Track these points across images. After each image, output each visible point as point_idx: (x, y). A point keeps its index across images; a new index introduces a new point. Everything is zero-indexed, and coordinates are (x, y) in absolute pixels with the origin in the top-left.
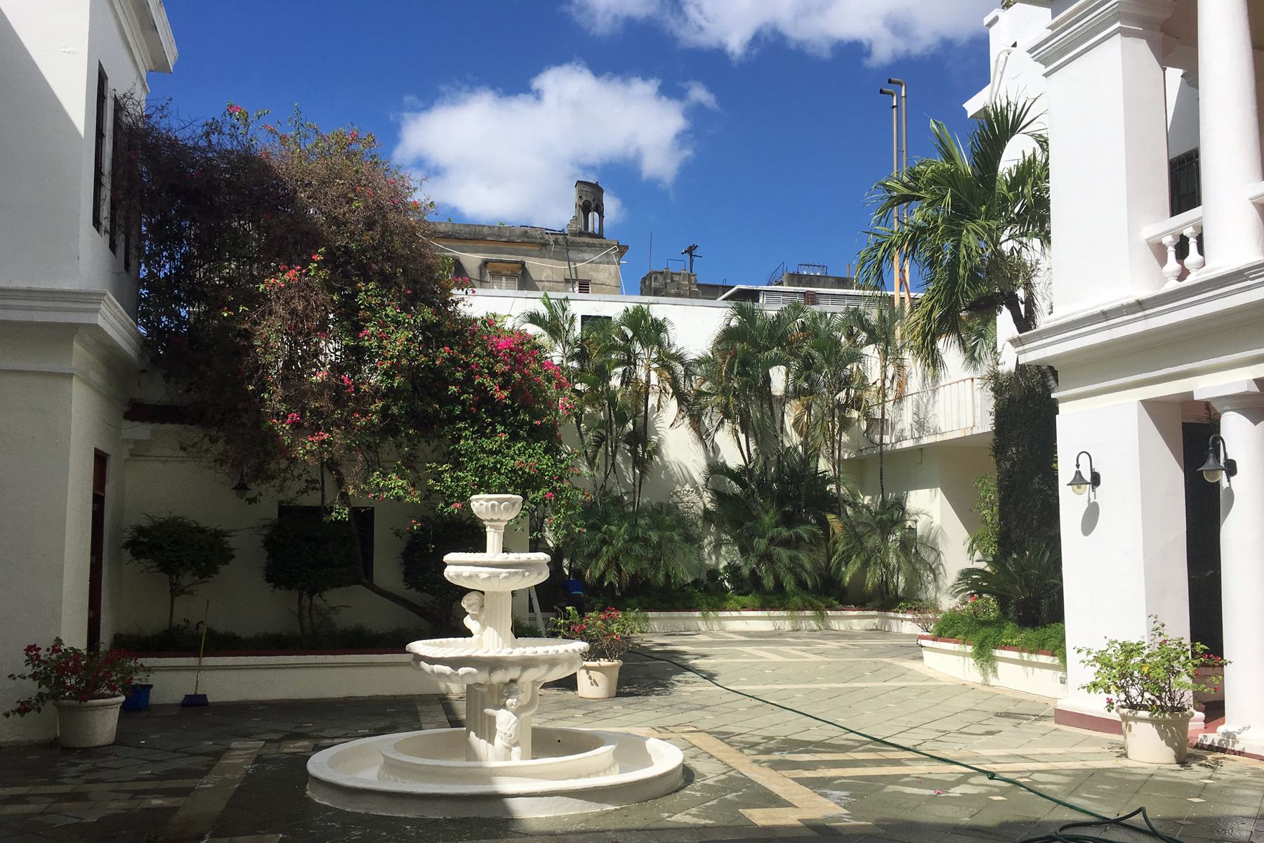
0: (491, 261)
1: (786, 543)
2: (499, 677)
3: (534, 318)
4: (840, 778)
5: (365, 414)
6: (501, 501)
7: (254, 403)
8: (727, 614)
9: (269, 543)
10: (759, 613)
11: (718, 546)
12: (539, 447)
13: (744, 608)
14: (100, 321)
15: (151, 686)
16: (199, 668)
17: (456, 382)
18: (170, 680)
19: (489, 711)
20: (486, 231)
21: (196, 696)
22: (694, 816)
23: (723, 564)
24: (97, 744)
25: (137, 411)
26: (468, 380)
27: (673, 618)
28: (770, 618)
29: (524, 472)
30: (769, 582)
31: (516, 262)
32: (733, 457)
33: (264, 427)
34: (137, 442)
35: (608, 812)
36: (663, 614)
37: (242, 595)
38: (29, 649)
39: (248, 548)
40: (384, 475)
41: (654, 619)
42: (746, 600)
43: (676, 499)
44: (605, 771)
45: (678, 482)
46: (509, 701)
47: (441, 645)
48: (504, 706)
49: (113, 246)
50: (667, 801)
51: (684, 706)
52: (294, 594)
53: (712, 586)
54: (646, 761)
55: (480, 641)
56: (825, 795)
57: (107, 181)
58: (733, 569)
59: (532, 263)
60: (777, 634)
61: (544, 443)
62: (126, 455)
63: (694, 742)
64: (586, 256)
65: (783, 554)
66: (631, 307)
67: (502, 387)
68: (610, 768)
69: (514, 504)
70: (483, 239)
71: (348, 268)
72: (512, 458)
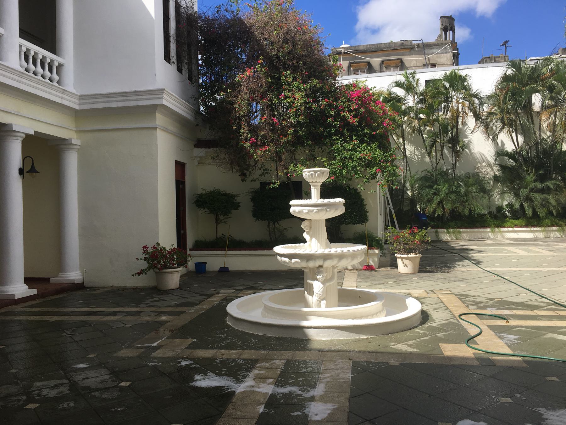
0: (385, 60)
1: (542, 191)
2: (311, 264)
3: (398, 84)
4: (519, 327)
5: (286, 136)
6: (315, 172)
7: (236, 135)
8: (506, 229)
9: (253, 199)
10: (525, 229)
11: (503, 193)
12: (374, 146)
13: (516, 226)
14: (164, 102)
15: (206, 263)
16: (226, 256)
17: (331, 116)
18: (215, 261)
19: (310, 281)
20: (383, 46)
21: (224, 268)
22: (410, 346)
23: (505, 203)
24: (170, 288)
25: (199, 144)
26: (337, 115)
27: (475, 232)
28: (531, 231)
29: (366, 159)
30: (529, 212)
31: (398, 59)
32: (510, 147)
33: (240, 145)
34: (200, 157)
35: (362, 340)
36: (469, 230)
37: (243, 224)
38: (145, 247)
39: (245, 201)
40: (296, 165)
41: (464, 232)
42: (516, 222)
43: (477, 171)
44: (372, 315)
45: (479, 162)
46: (318, 277)
47: (292, 248)
48: (317, 279)
49: (179, 70)
50: (393, 337)
51: (452, 279)
52: (267, 222)
53: (499, 215)
54: (405, 308)
55: (310, 245)
56: (501, 338)
57: (172, 39)
58: (510, 206)
59: (405, 58)
60: (535, 240)
61: (377, 143)
62: (197, 163)
63: (443, 300)
64: (434, 51)
65: (538, 197)
66: (448, 73)
67: (354, 117)
68: (376, 314)
69: (323, 173)
70: (382, 50)
71: (275, 66)
72: (360, 153)
